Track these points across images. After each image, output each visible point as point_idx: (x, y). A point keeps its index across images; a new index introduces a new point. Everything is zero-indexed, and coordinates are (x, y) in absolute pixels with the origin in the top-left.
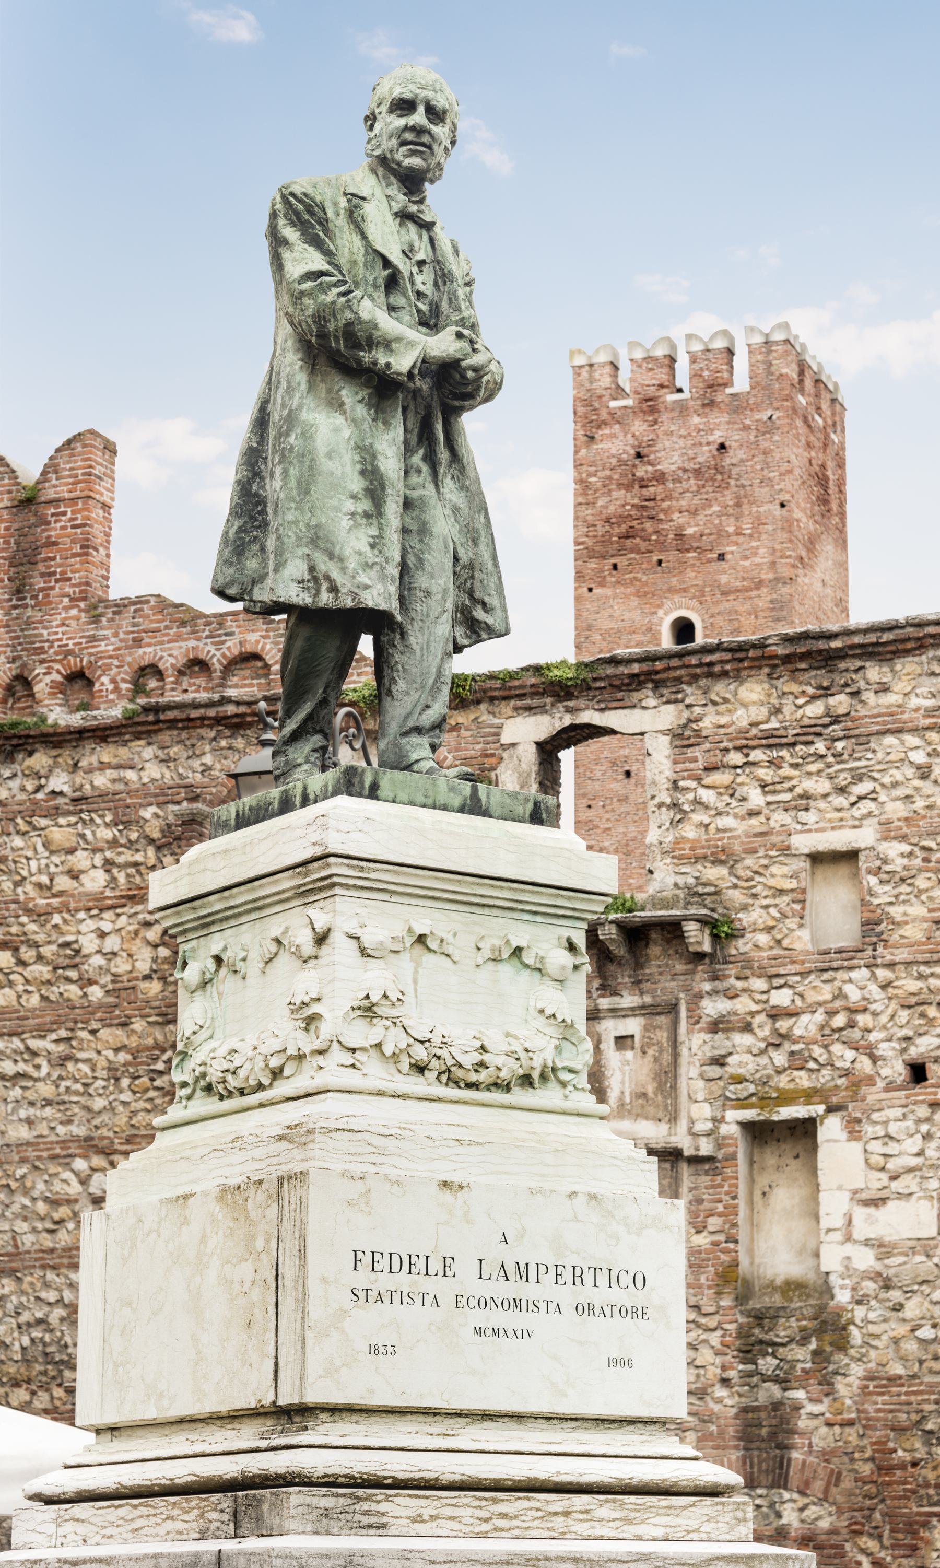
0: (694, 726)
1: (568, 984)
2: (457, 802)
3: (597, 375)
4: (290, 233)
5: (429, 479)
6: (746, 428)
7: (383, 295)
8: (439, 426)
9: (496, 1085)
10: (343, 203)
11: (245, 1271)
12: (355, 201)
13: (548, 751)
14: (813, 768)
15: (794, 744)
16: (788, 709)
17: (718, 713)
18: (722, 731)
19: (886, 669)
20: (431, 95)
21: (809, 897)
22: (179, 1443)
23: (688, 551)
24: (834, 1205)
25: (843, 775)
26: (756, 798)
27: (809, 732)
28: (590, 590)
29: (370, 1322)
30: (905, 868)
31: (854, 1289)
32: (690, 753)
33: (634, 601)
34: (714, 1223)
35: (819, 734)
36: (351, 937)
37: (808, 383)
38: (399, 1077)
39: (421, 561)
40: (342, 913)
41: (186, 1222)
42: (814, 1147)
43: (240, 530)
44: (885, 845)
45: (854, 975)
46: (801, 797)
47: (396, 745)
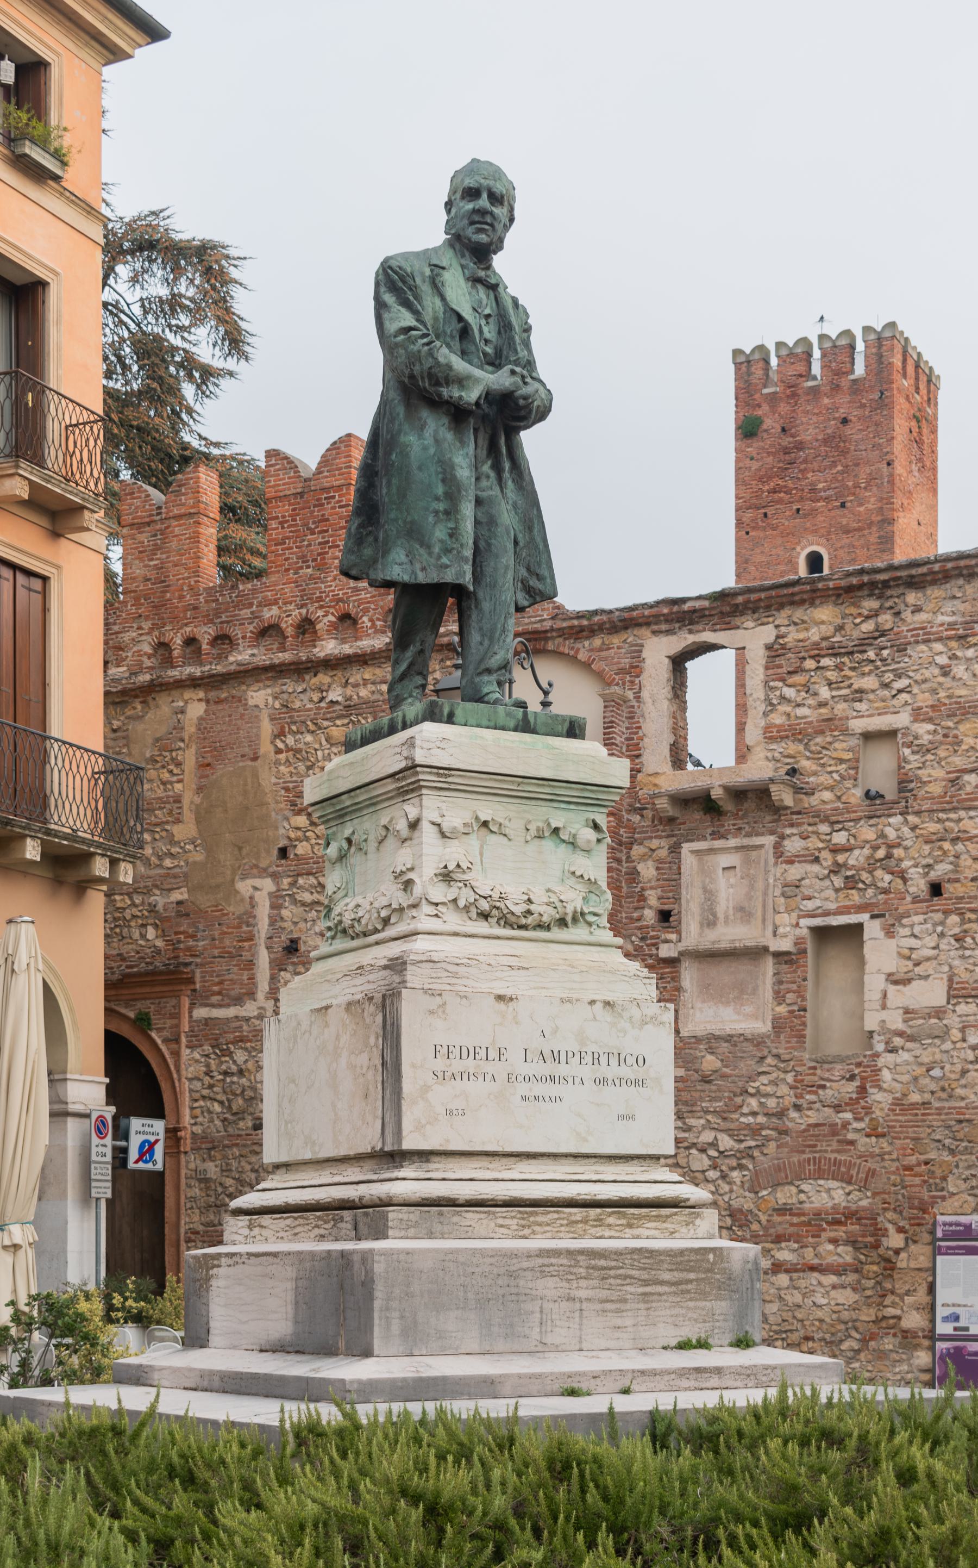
0: (781, 641)
1: (594, 853)
2: (512, 724)
3: (753, 369)
4: (389, 298)
5: (495, 482)
6: (863, 406)
7: (458, 344)
8: (502, 441)
9: (539, 926)
10: (427, 272)
11: (363, 1059)
12: (437, 270)
13: (679, 662)
14: (867, 669)
15: (852, 653)
16: (848, 627)
17: (797, 631)
18: (801, 644)
19: (920, 595)
20: (491, 183)
21: (861, 765)
22: (325, 1176)
23: (818, 501)
24: (874, 983)
25: (887, 675)
26: (825, 693)
27: (864, 643)
28: (747, 533)
29: (442, 1095)
30: (930, 742)
31: (887, 1043)
32: (777, 661)
33: (779, 541)
34: (790, 997)
35: (871, 645)
36: (433, 823)
37: (910, 369)
38: (470, 922)
39: (489, 545)
40: (431, 806)
41: (327, 1025)
42: (861, 943)
43: (361, 526)
44: (916, 725)
45: (891, 820)
46: (857, 691)
47: (473, 682)
